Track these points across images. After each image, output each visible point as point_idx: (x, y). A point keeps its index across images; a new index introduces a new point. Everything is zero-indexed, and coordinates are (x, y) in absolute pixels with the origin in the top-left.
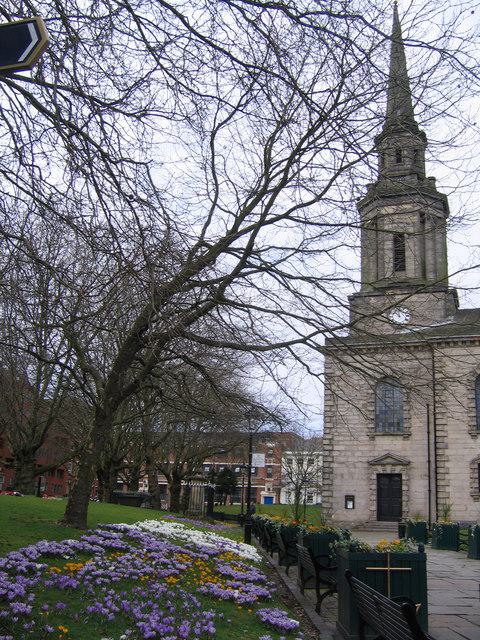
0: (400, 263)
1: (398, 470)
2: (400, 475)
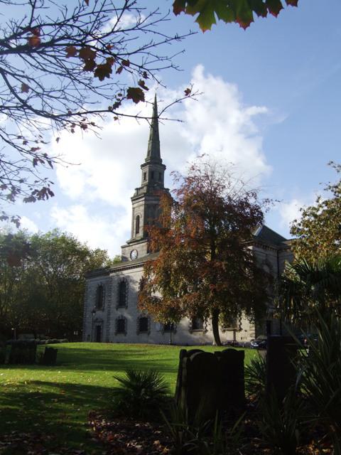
0: (137, 232)
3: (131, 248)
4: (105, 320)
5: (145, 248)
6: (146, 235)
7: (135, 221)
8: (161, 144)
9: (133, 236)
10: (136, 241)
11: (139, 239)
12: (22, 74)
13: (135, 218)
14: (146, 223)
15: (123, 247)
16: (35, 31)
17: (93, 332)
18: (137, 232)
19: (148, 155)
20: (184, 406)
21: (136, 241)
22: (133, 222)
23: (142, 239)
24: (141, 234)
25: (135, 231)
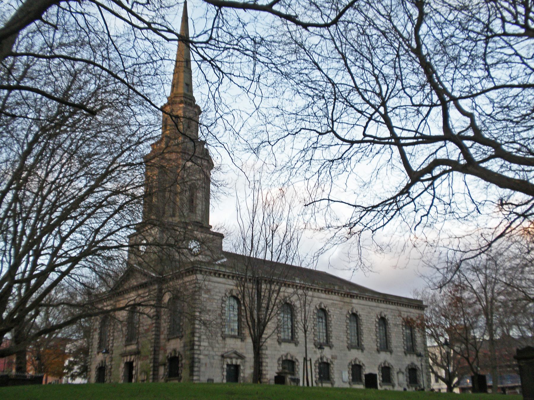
1: (239, 362)
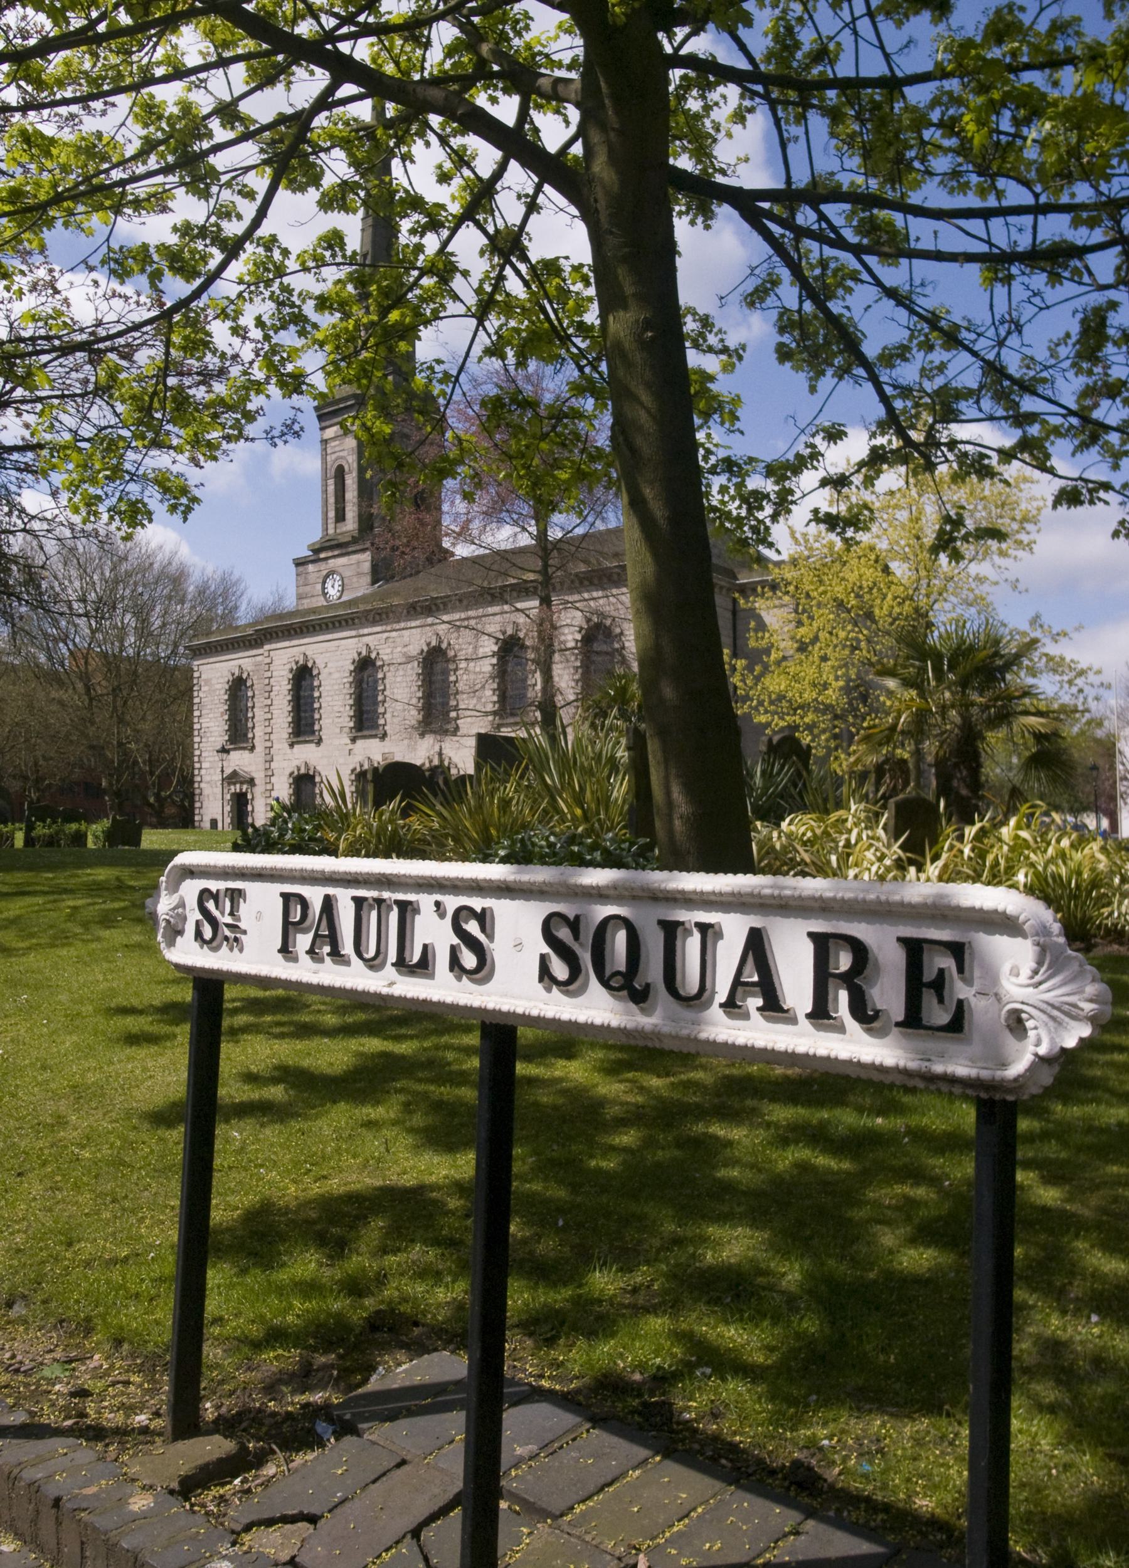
0: (340, 517)
2: (245, 794)
3: (324, 567)
4: (259, 777)
5: (367, 566)
6: (366, 523)
7: (331, 482)
8: (679, 275)
9: (326, 529)
10: (339, 546)
11: (348, 539)
12: (122, 327)
13: (332, 472)
14: (366, 490)
15: (300, 563)
16: (939, 318)
17: (228, 808)
18: (340, 517)
19: (485, 880)
20: (621, 1081)
21: (339, 546)
22: (325, 486)
23: (355, 540)
24: (351, 524)
25: (332, 514)
